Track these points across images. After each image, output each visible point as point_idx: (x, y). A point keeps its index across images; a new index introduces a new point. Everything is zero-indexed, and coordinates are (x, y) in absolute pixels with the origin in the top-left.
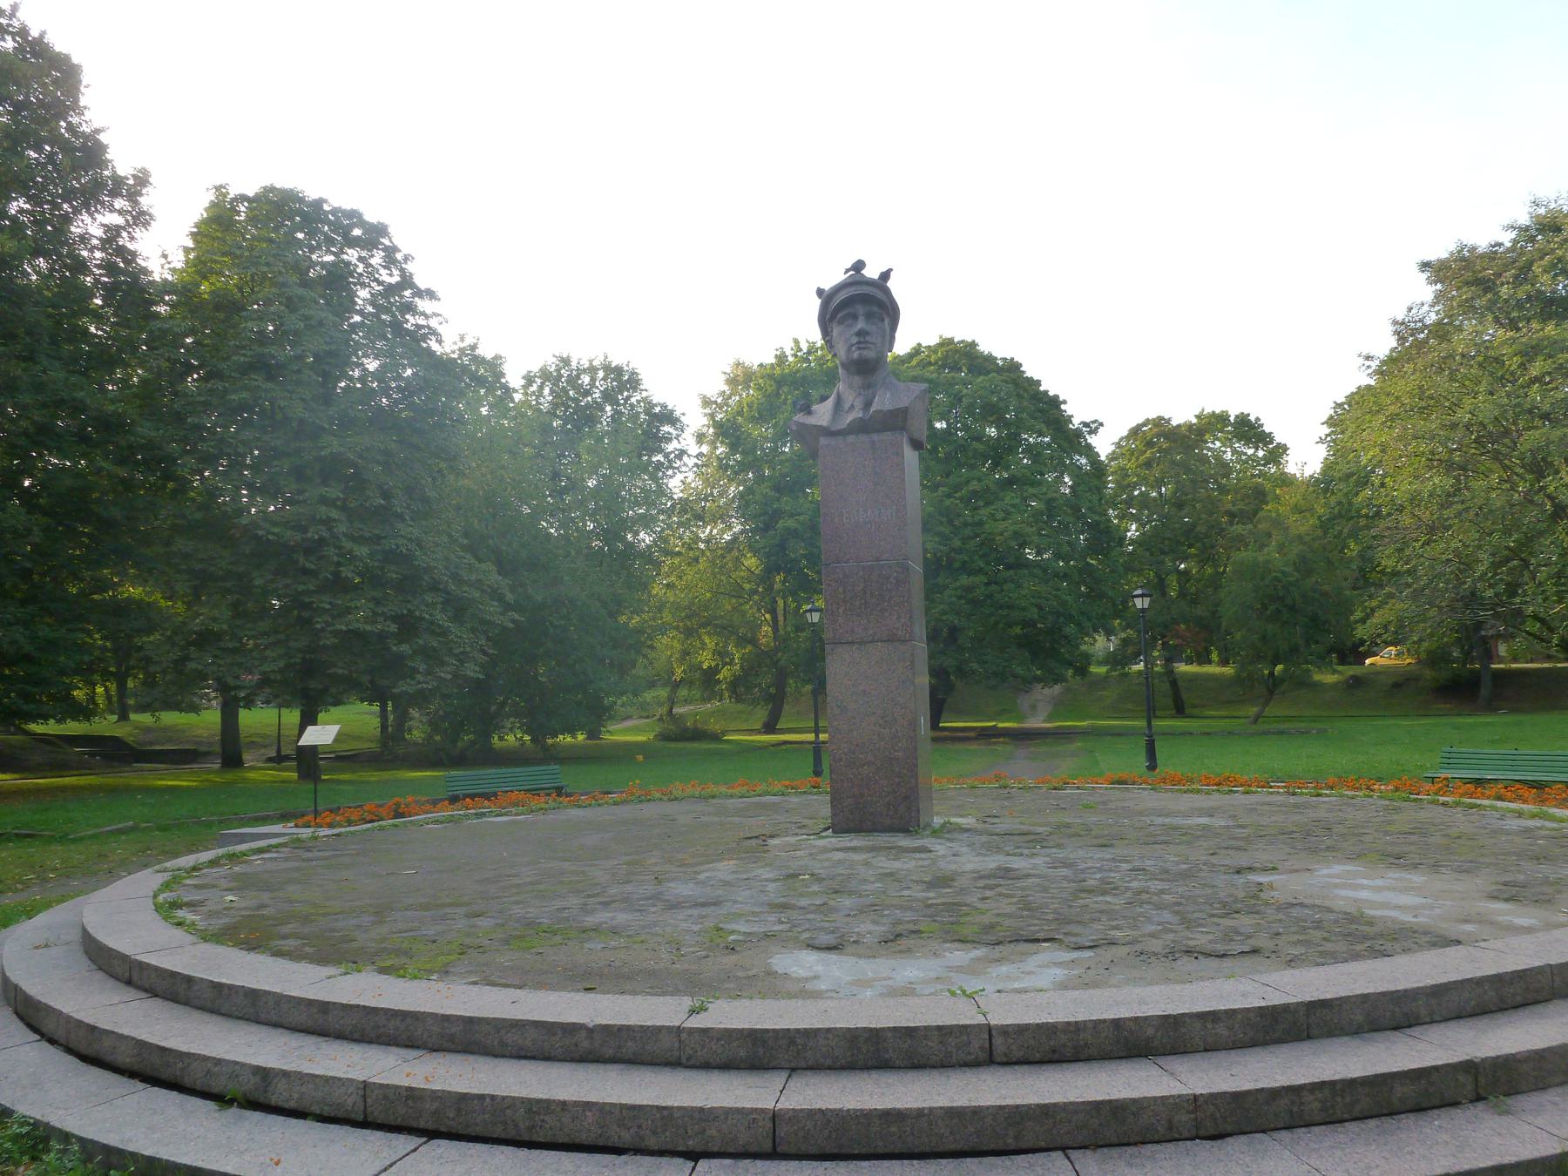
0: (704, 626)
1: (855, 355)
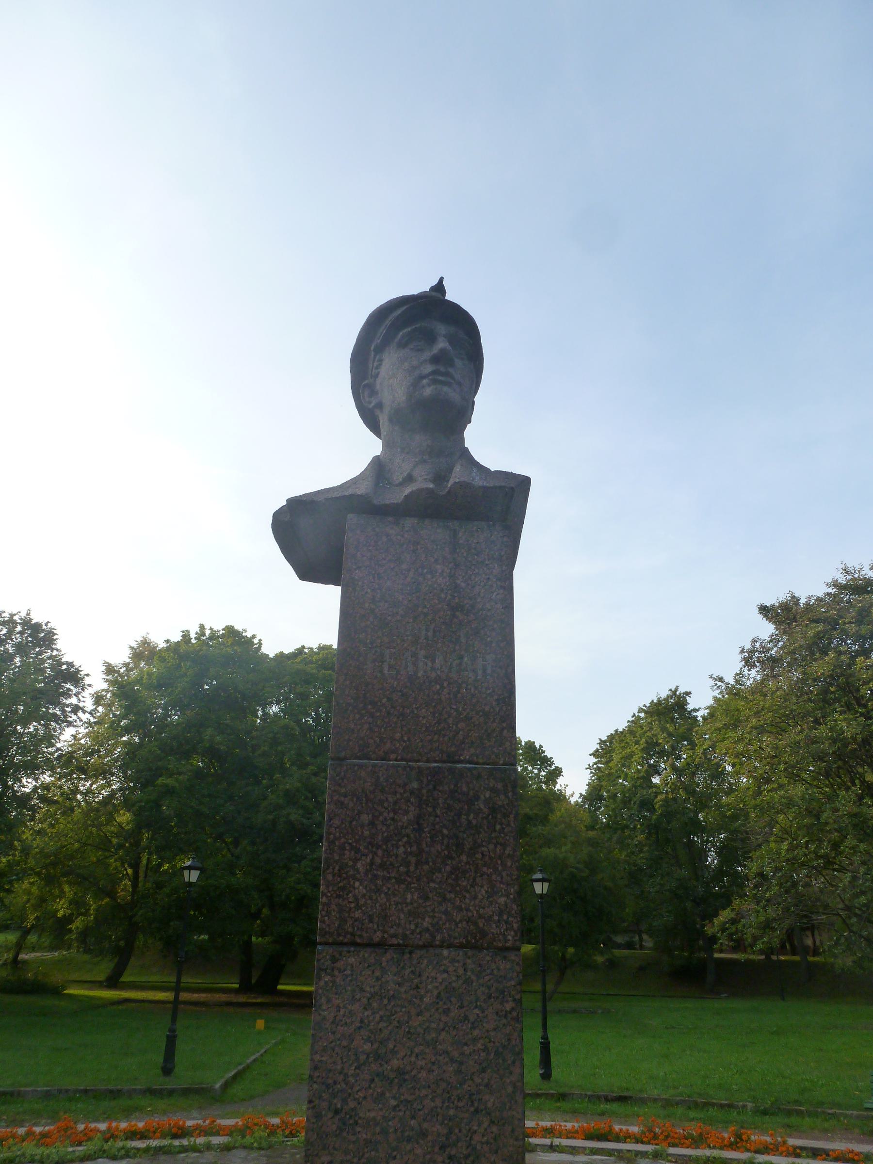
0: (66, 874)
1: (428, 391)
